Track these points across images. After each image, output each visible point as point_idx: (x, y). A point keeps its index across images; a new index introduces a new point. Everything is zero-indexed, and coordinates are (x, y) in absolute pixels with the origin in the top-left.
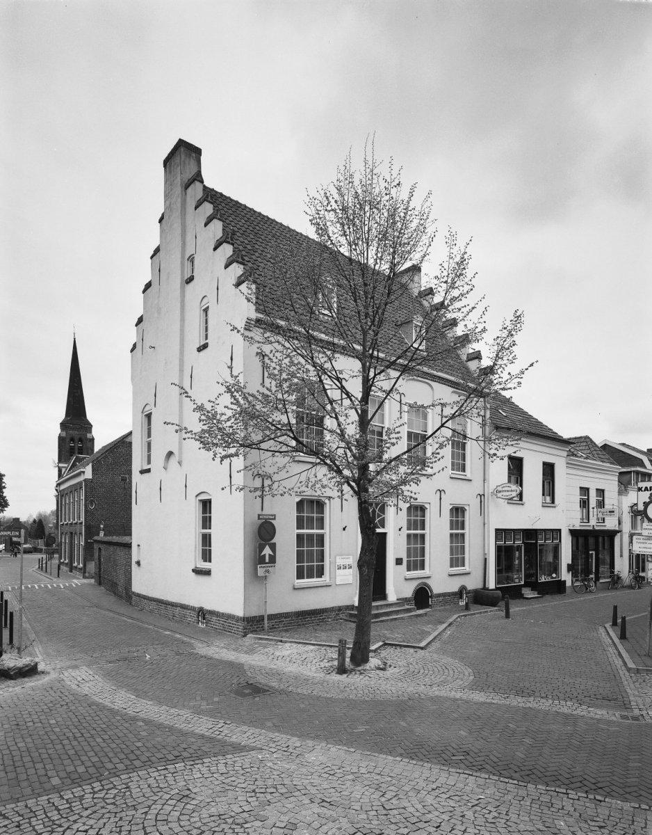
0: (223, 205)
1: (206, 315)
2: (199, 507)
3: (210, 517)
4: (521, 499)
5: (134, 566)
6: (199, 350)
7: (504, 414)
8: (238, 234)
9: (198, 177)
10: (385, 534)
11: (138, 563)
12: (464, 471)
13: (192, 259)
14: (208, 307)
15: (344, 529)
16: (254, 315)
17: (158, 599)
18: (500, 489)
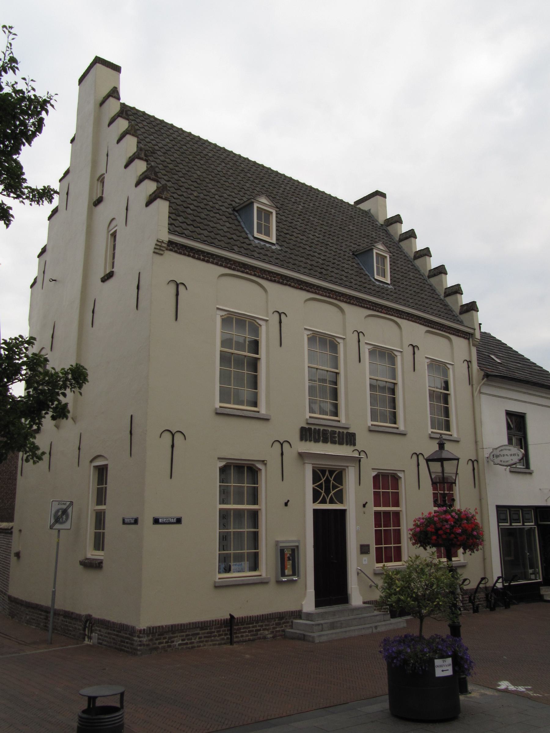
0: (145, 123)
1: (115, 240)
2: (92, 477)
3: (106, 488)
4: (528, 466)
5: (13, 559)
6: (104, 280)
7: (498, 361)
8: (159, 153)
9: (114, 93)
10: (343, 512)
11: (18, 555)
12: (395, 423)
13: (101, 179)
14: (116, 232)
15: (286, 504)
16: (165, 236)
17: (37, 605)
18: (497, 452)
